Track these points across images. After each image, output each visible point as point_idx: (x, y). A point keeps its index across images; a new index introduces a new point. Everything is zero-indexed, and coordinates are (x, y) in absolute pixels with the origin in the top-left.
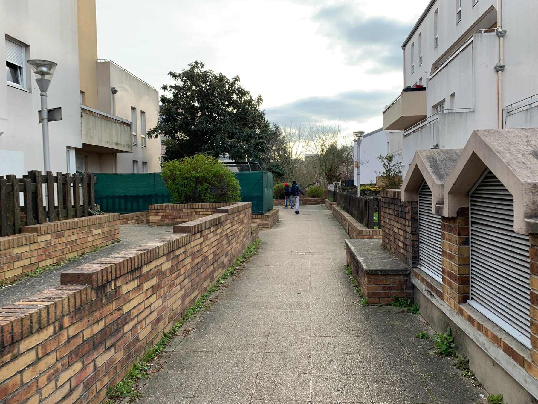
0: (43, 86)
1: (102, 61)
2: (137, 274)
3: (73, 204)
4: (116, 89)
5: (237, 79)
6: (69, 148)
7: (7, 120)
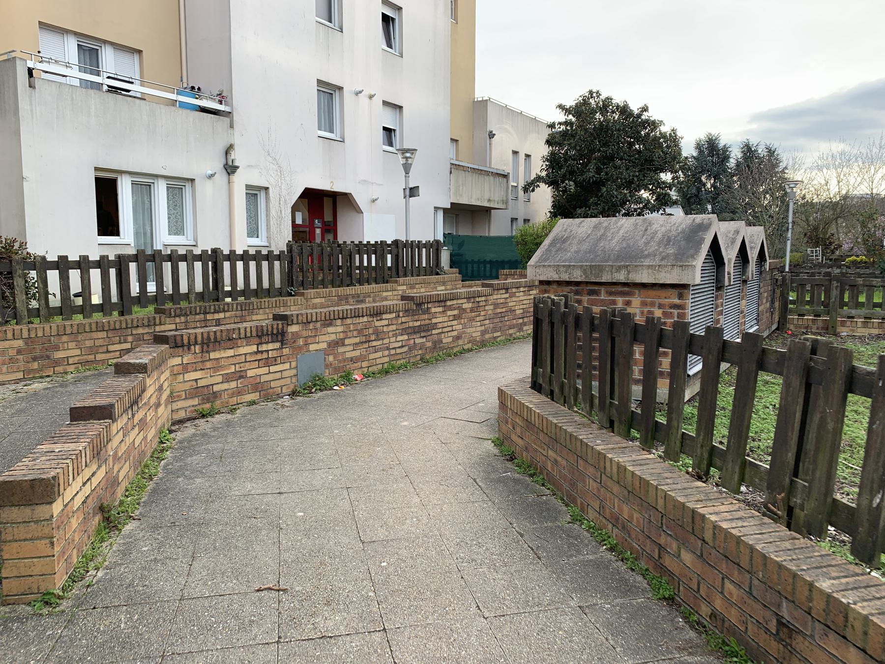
0: (407, 168)
1: (479, 99)
2: (443, 304)
3: (417, 266)
4: (494, 133)
5: (645, 109)
6: (436, 209)
7: (382, 185)
